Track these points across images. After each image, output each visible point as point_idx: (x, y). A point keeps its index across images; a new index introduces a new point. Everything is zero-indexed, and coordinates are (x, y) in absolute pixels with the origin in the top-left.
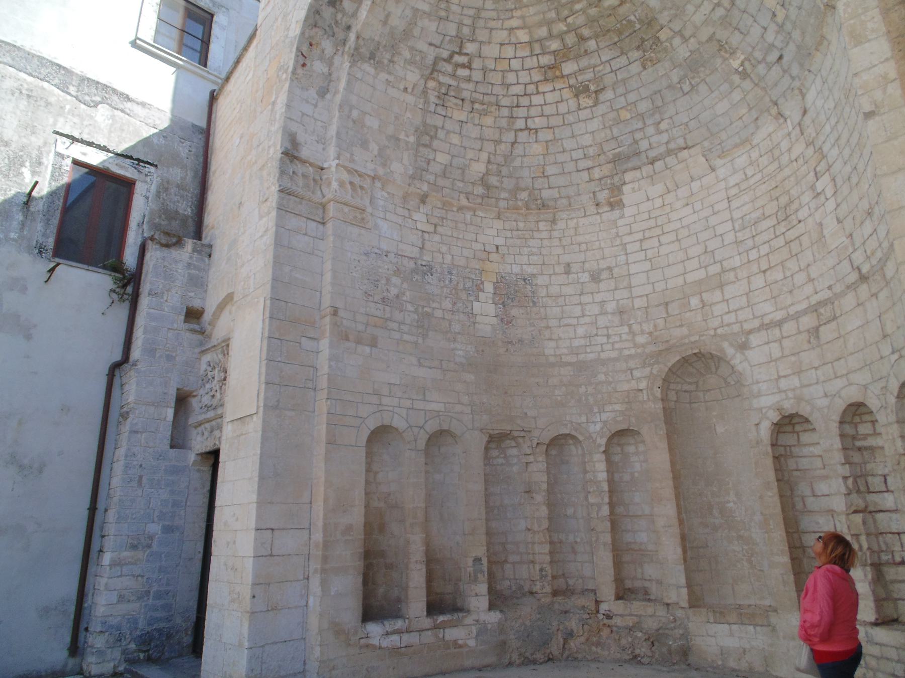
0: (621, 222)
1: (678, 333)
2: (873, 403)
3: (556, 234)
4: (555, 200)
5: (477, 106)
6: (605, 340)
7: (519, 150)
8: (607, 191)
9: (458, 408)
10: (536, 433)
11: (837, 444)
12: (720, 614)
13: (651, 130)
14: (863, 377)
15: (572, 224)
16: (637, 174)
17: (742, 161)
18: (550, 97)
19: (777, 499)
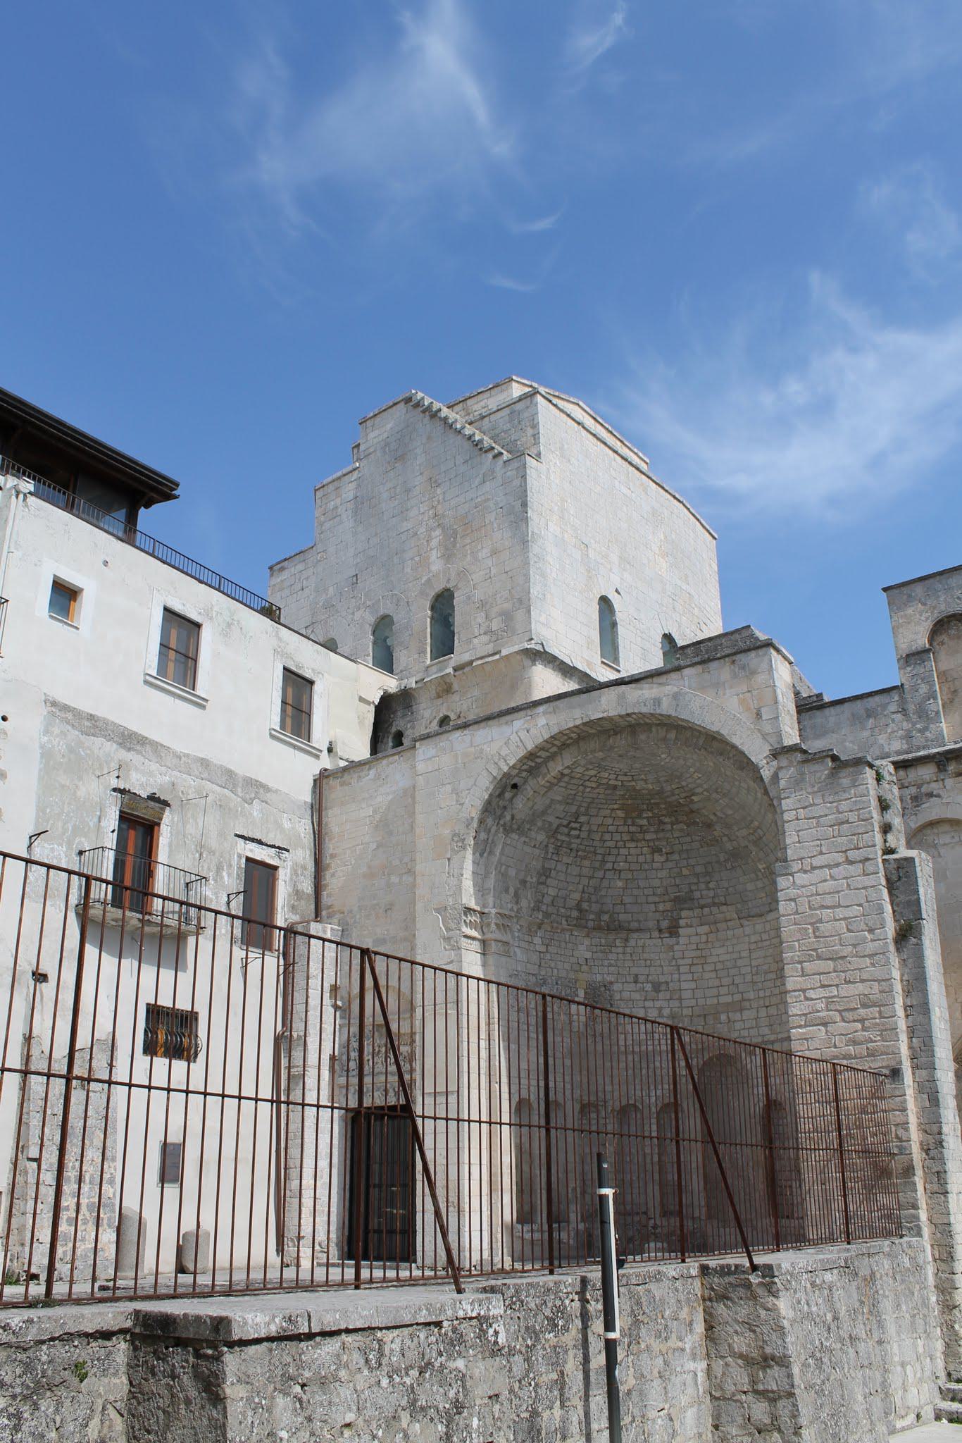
0: (676, 948)
3: (628, 950)
7: (605, 883)
15: (640, 943)
16: (690, 913)
17: (759, 927)
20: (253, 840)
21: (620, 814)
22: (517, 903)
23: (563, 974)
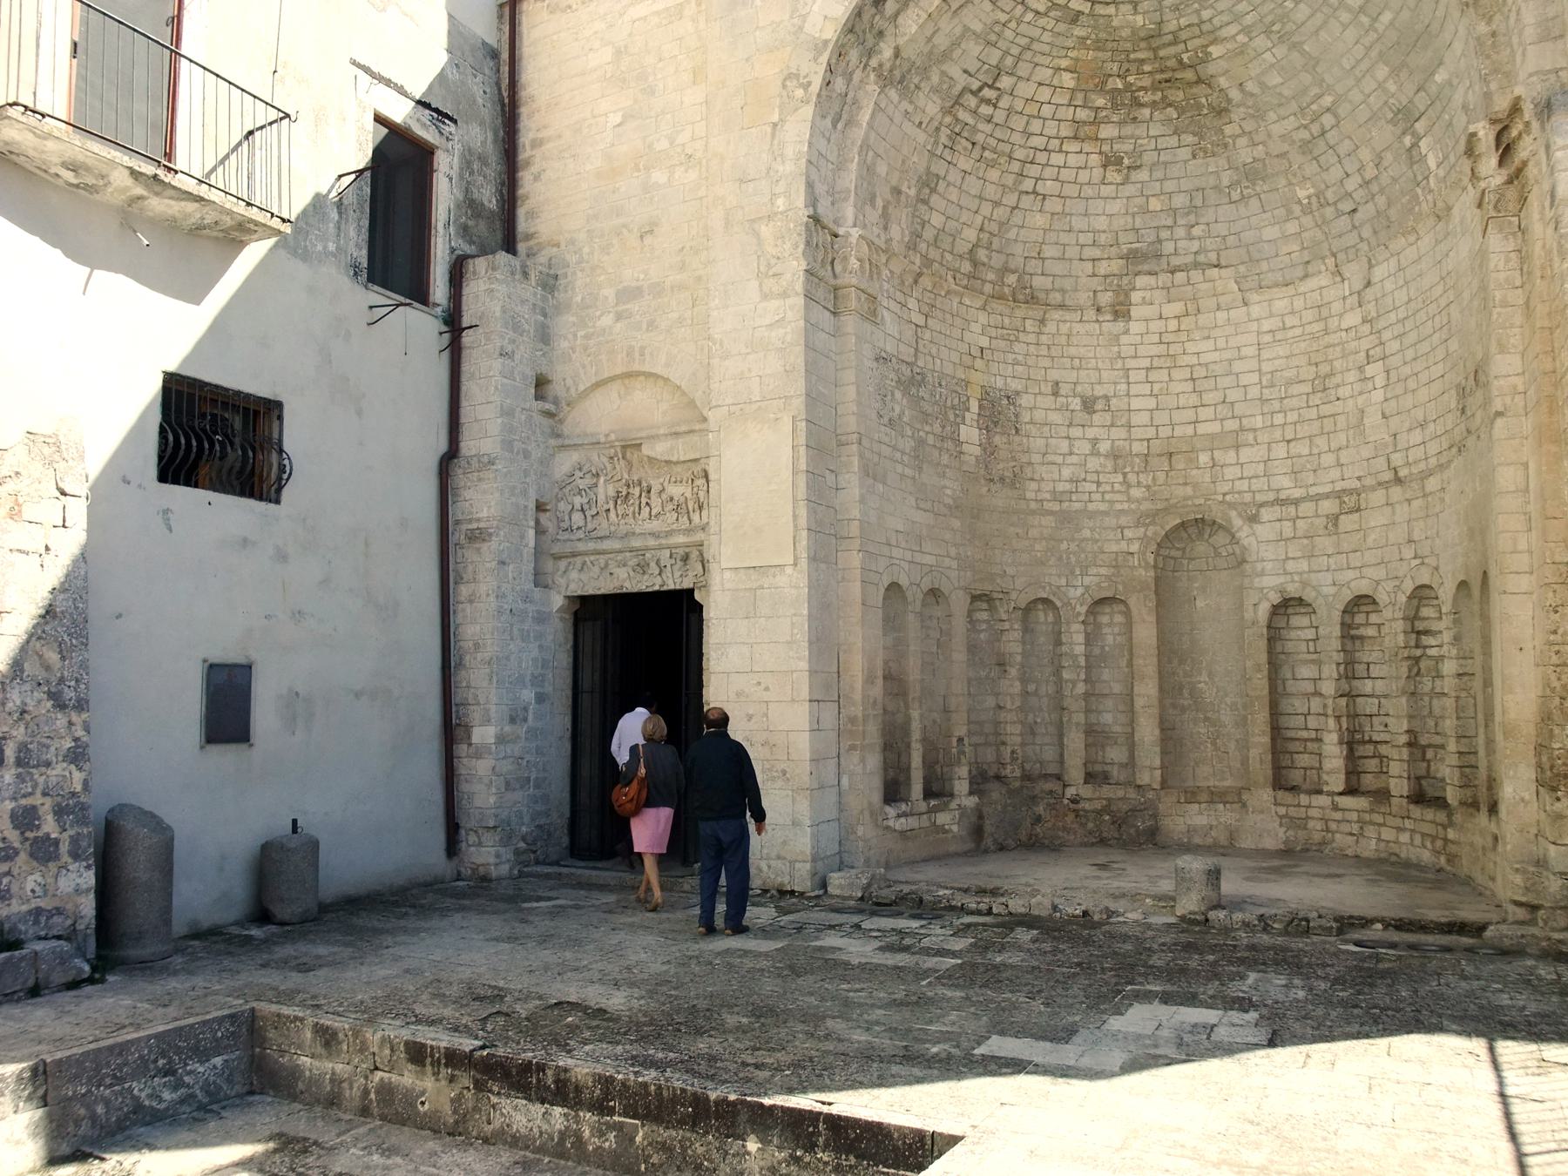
0: (1124, 339)
1: (1180, 492)
2: (1382, 597)
3: (1044, 339)
4: (1047, 292)
5: (987, 154)
6: (1094, 487)
7: (1017, 218)
8: (1110, 294)
9: (947, 562)
10: (1014, 595)
11: (1337, 631)
12: (1191, 796)
13: (1180, 232)
14: (1379, 573)
15: (1064, 328)
16: (1151, 280)
17: (1280, 305)
18: (1073, 160)
19: (1265, 682)
20: (388, 83)
21: (1068, 80)
22: (886, 228)
23: (949, 370)
